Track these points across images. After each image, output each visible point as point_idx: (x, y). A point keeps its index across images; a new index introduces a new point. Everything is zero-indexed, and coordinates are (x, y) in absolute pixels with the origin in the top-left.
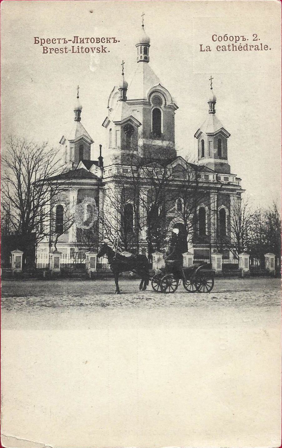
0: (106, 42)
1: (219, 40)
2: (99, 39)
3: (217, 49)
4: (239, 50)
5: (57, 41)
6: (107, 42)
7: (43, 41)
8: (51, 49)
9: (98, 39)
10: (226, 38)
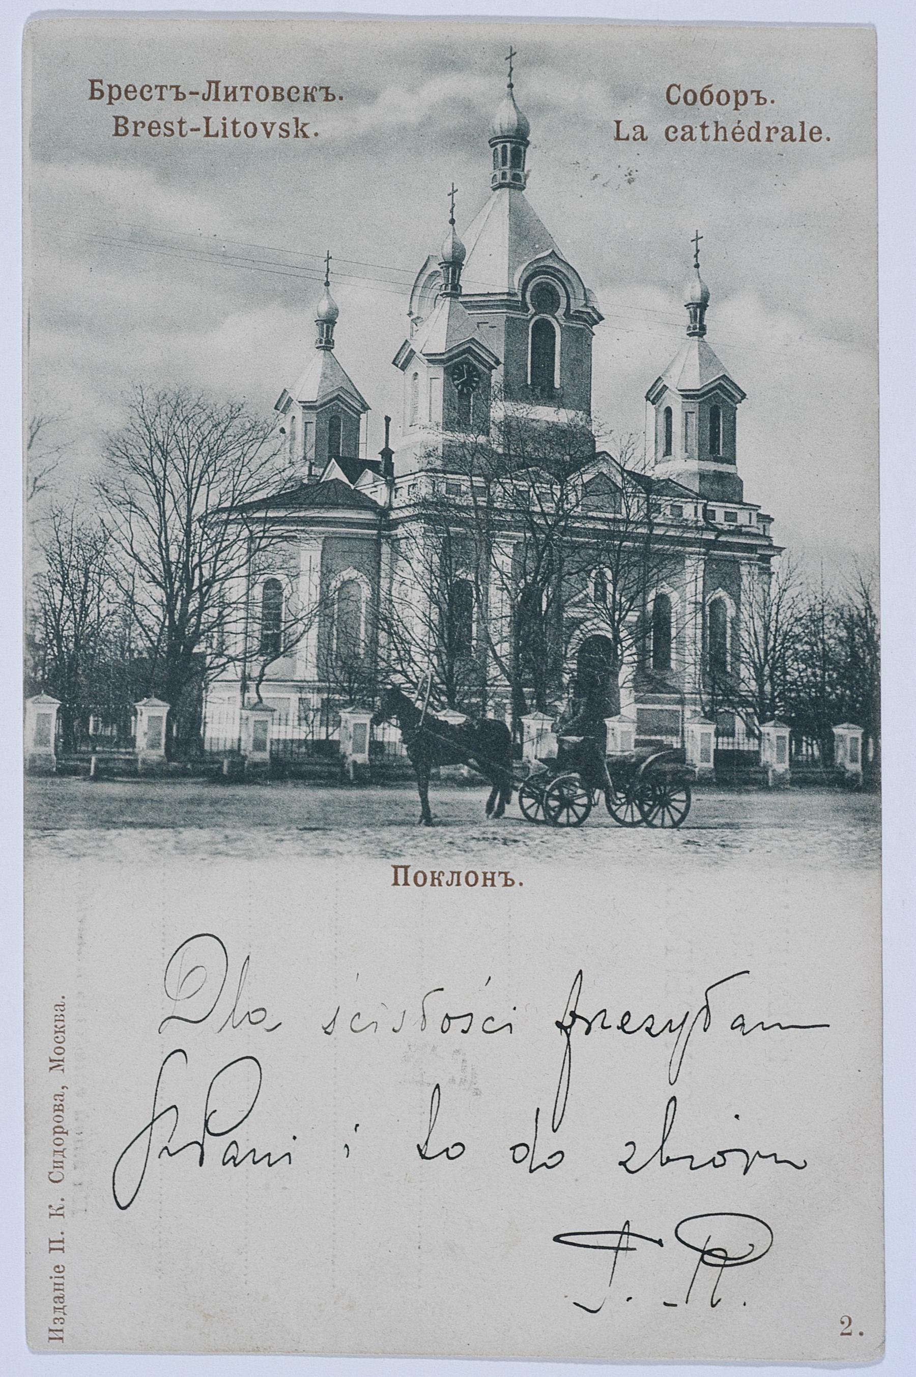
2: (282, 90)
4: (735, 140)
5: (156, 93)
6: (63, 1032)
7: (115, 90)
8: (136, 124)
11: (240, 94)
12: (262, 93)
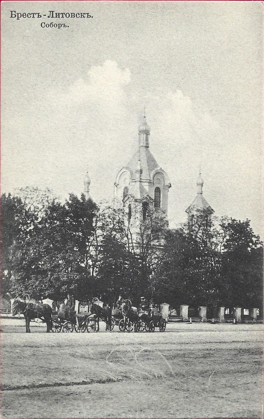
0: (80, 17)
1: (46, 26)
2: (74, 14)
3: (41, 25)
5: (32, 16)
7: (19, 15)
9: (73, 14)
10: (51, 25)
11: (61, 16)
12: (68, 15)
